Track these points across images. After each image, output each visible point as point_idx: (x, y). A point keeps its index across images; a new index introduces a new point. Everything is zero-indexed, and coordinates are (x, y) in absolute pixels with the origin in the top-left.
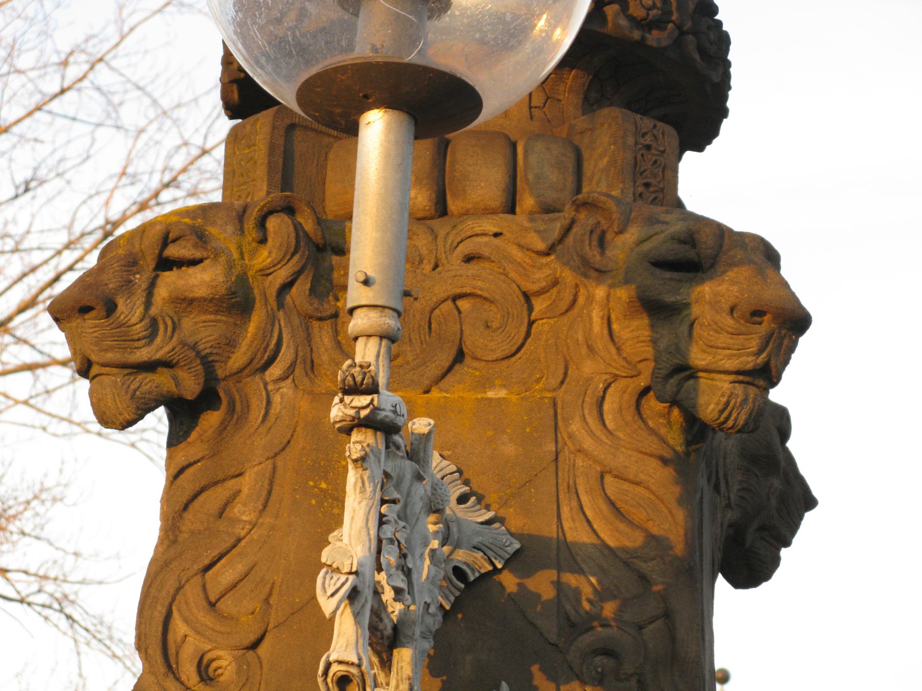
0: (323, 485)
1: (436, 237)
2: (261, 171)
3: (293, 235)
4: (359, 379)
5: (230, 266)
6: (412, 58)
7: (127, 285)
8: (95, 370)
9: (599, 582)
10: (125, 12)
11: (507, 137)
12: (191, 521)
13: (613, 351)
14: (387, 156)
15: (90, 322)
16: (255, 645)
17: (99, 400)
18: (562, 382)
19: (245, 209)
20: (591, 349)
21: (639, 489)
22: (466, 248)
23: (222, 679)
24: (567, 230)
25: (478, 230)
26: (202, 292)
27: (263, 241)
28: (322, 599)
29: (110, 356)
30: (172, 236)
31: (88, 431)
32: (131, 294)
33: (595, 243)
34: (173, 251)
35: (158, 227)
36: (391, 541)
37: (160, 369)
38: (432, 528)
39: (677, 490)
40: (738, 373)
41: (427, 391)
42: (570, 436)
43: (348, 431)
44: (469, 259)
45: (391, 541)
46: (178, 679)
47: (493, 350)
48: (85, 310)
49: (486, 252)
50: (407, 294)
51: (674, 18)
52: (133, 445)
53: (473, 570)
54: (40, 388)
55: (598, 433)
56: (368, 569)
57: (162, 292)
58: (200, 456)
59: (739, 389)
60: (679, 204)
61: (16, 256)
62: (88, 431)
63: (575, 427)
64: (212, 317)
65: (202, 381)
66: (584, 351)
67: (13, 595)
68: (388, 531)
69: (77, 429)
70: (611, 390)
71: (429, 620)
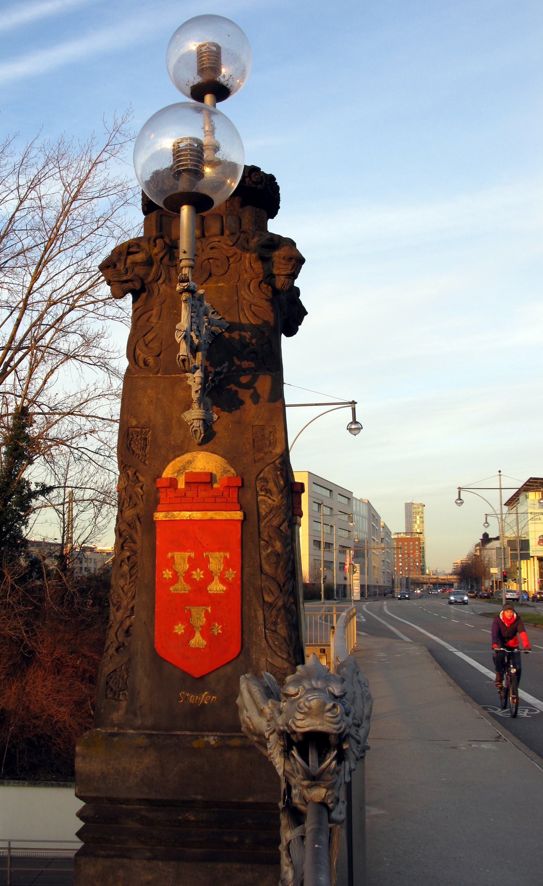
0: (175, 312)
1: (202, 243)
2: (154, 228)
3: (163, 244)
4: (184, 278)
5: (147, 253)
6: (194, 190)
7: (119, 260)
8: (112, 283)
9: (251, 334)
10: (113, 206)
11: (221, 215)
12: (140, 323)
13: (252, 271)
14: (188, 218)
15: (110, 270)
16: (159, 355)
17: (113, 291)
18: (239, 280)
19: (150, 238)
20: (246, 271)
21: (261, 309)
22: (211, 245)
23: (150, 365)
24: (238, 239)
25: (214, 240)
26: (139, 261)
27: (155, 246)
28: (177, 339)
29: (116, 279)
30: (130, 246)
31: (109, 318)
32: (120, 262)
33: (246, 242)
34: (131, 250)
35: (127, 244)
36: (195, 322)
37: (129, 282)
38: (206, 320)
39: (271, 308)
40: (286, 275)
41: (202, 285)
42: (241, 295)
43: (181, 293)
44: (212, 248)
45: (195, 322)
46: (138, 365)
47: (219, 273)
48: (108, 267)
49: (216, 246)
50: (196, 255)
51: (264, 181)
52: (121, 322)
53: (217, 332)
54: (96, 307)
55: (249, 294)
56: (189, 330)
57: (129, 261)
58: (141, 305)
59: (287, 280)
60: (268, 231)
61: (87, 273)
62: (109, 318)
63: (243, 292)
64: (142, 267)
65: (141, 284)
66: (244, 271)
67: (91, 363)
68: (194, 320)
69: (106, 318)
70: (252, 282)
71: (206, 346)
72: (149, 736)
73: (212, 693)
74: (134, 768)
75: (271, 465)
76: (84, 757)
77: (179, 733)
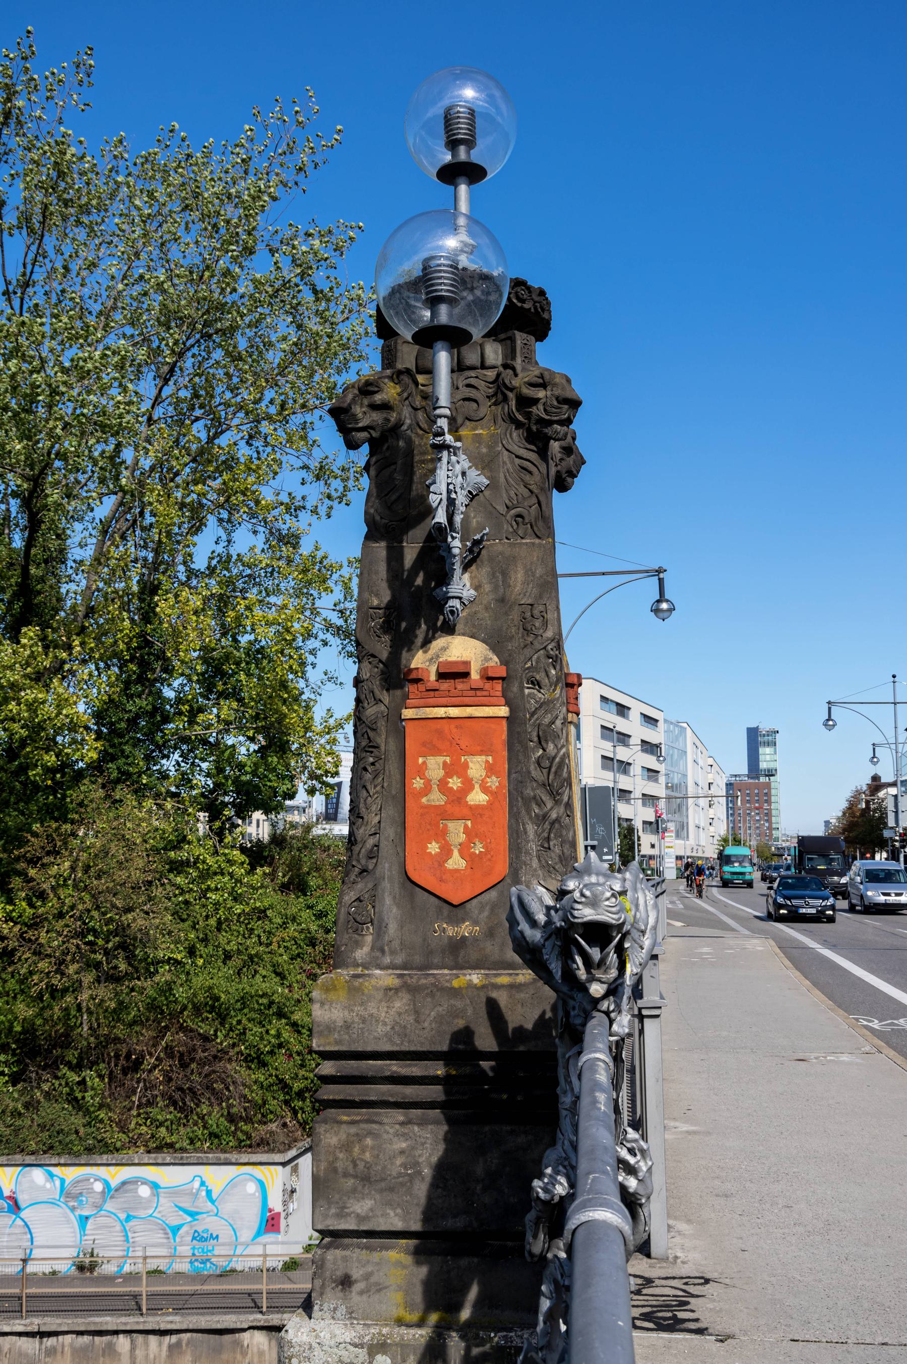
72: (400, 976)
73: (475, 923)
74: (383, 1014)
75: (542, 652)
76: (322, 1004)
77: (435, 972)
